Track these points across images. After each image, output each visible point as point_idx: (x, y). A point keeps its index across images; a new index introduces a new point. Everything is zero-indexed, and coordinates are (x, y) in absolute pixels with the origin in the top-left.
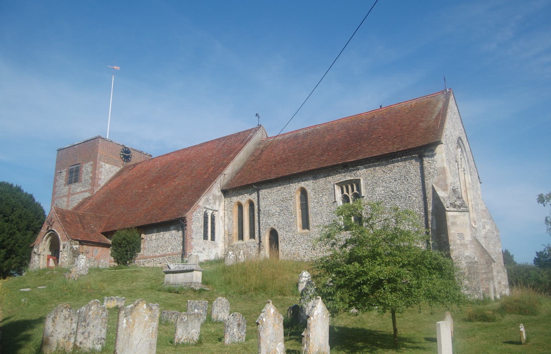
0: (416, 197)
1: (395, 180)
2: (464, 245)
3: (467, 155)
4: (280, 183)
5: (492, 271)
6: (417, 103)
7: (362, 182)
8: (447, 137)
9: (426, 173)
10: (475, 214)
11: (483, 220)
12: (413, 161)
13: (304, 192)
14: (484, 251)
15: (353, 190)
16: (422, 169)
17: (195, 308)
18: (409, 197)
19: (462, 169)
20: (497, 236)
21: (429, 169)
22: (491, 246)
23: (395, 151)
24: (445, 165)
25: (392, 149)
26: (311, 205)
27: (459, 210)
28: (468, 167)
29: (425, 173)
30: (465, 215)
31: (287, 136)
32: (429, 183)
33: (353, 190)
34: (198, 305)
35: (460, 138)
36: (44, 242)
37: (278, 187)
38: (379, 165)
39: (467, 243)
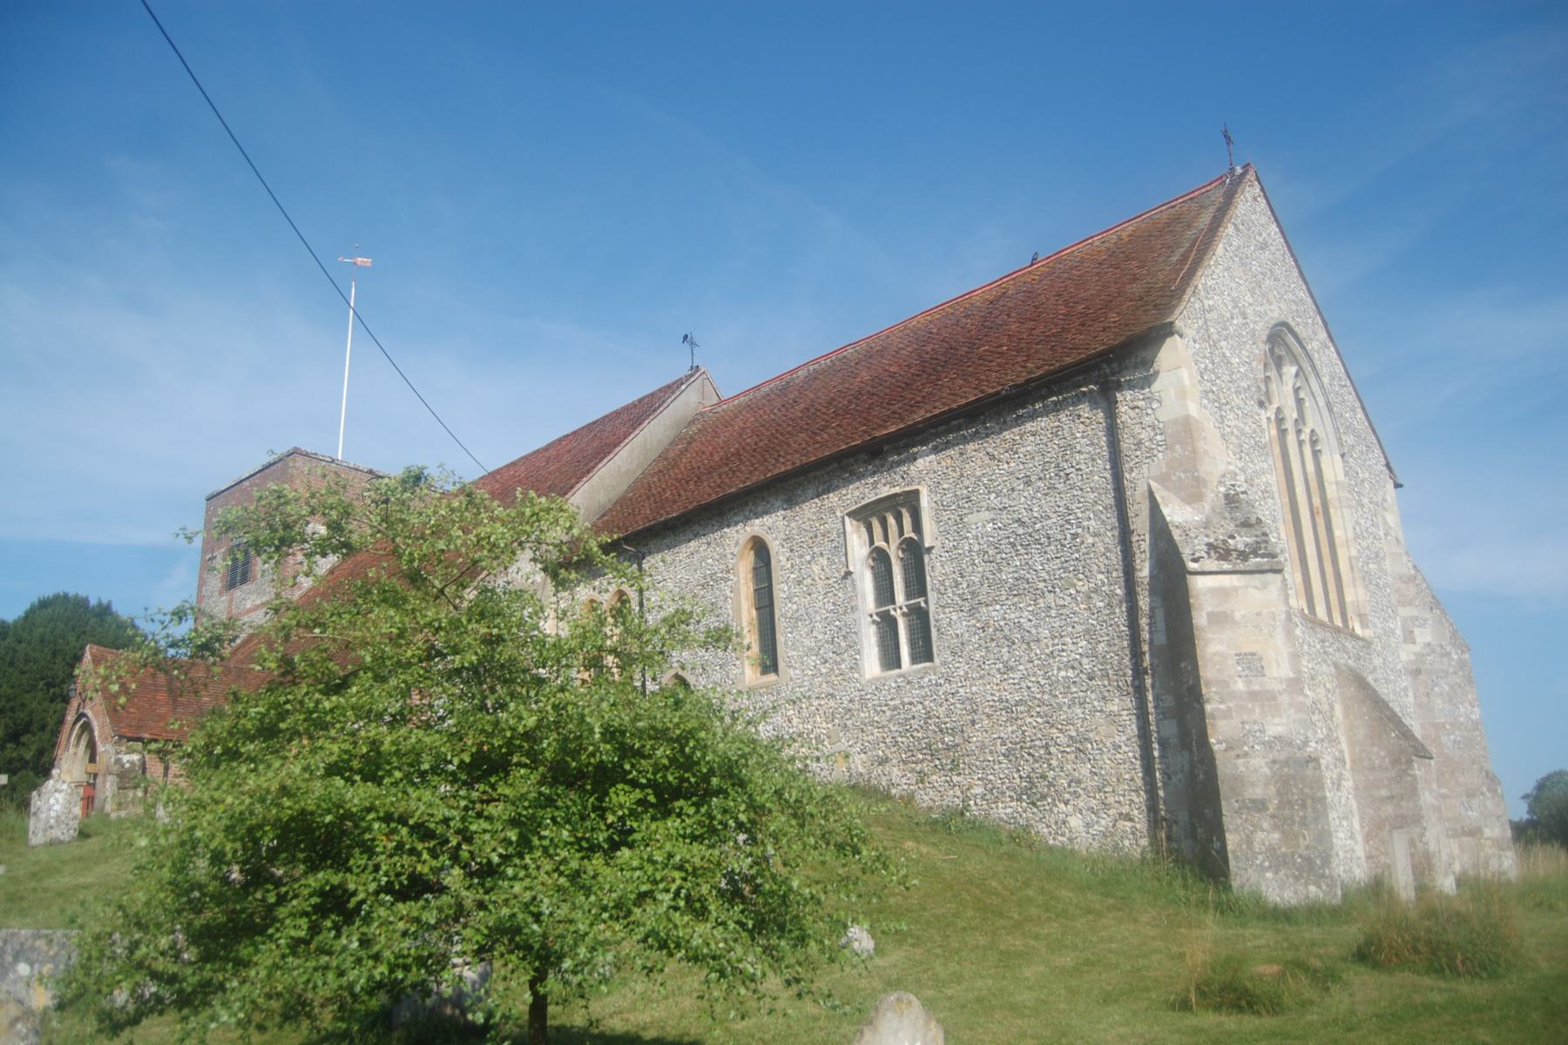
0: (1096, 535)
1: (1028, 483)
2: (1265, 698)
3: (1322, 386)
4: (696, 528)
5: (1412, 792)
6: (1138, 228)
7: (925, 502)
8: (1214, 315)
9: (1126, 444)
10: (1361, 591)
11: (1404, 612)
12: (1084, 410)
13: (760, 548)
14: (1383, 715)
15: (901, 532)
16: (1113, 432)
17: (16, 959)
18: (1075, 536)
19: (1305, 436)
20: (1462, 664)
21: (1137, 429)
22: (1439, 703)
23: (1021, 380)
24: (1193, 410)
25: (1016, 375)
26: (780, 591)
27: (1241, 567)
28: (1330, 429)
29: (1124, 445)
30: (1265, 586)
31: (766, 389)
32: (1139, 479)
33: (901, 532)
34: (33, 949)
35: (1285, 324)
36: (72, 750)
37: (692, 544)
38: (976, 436)
39: (1276, 687)
